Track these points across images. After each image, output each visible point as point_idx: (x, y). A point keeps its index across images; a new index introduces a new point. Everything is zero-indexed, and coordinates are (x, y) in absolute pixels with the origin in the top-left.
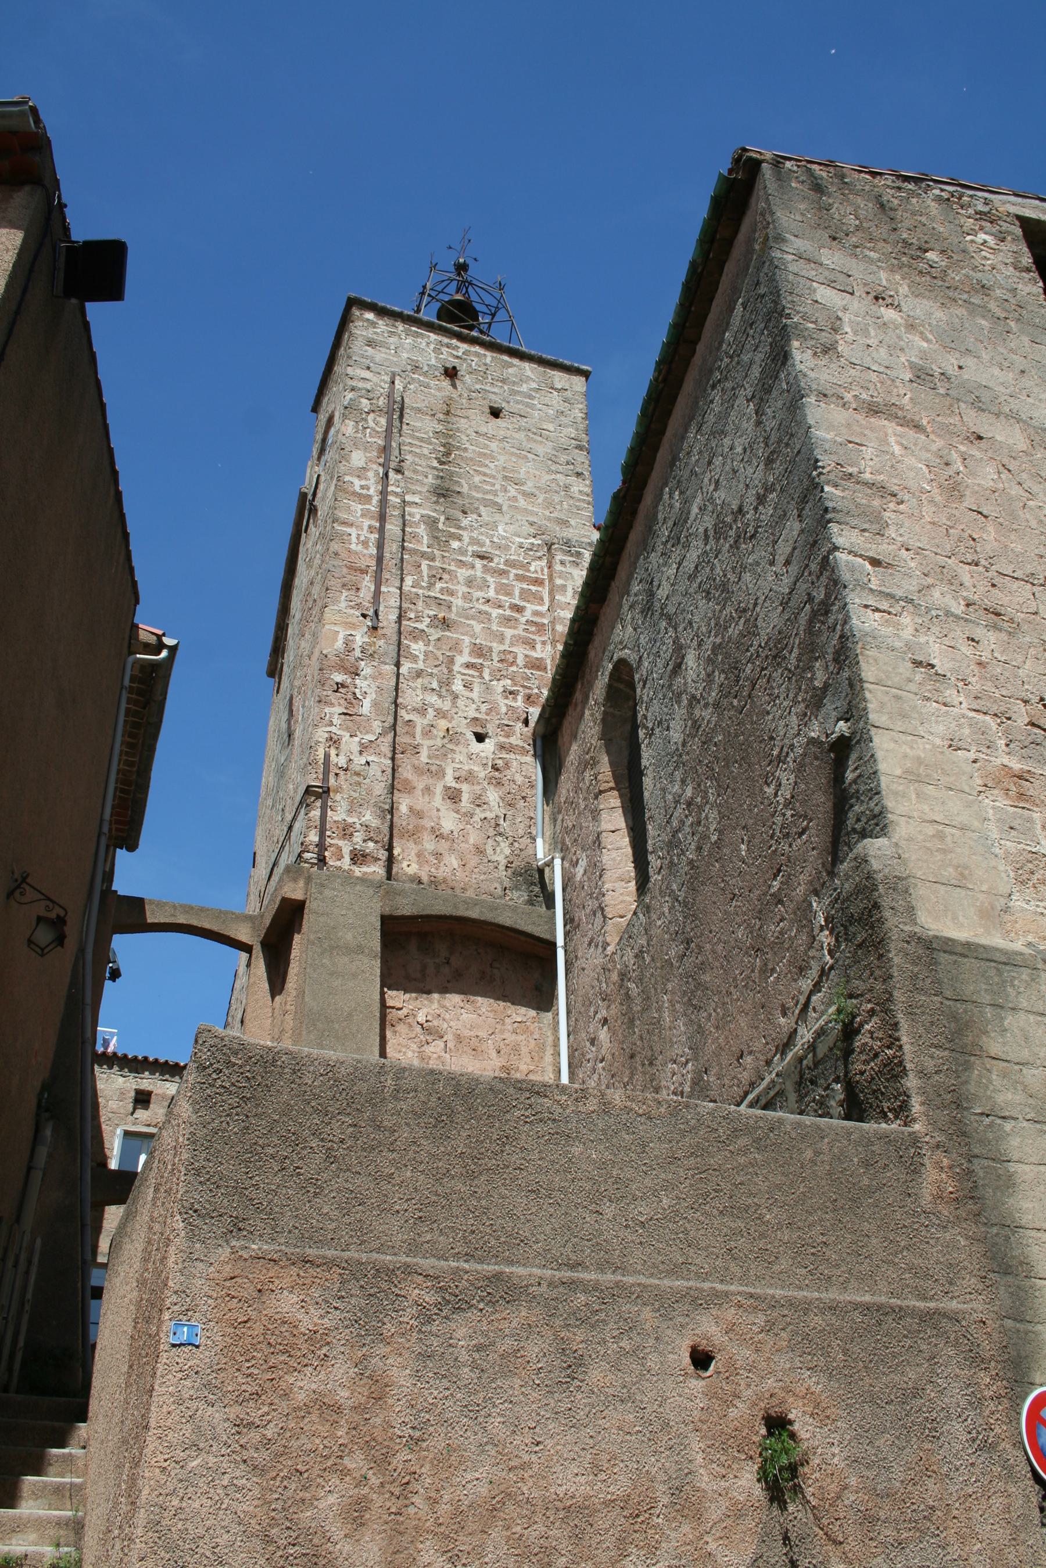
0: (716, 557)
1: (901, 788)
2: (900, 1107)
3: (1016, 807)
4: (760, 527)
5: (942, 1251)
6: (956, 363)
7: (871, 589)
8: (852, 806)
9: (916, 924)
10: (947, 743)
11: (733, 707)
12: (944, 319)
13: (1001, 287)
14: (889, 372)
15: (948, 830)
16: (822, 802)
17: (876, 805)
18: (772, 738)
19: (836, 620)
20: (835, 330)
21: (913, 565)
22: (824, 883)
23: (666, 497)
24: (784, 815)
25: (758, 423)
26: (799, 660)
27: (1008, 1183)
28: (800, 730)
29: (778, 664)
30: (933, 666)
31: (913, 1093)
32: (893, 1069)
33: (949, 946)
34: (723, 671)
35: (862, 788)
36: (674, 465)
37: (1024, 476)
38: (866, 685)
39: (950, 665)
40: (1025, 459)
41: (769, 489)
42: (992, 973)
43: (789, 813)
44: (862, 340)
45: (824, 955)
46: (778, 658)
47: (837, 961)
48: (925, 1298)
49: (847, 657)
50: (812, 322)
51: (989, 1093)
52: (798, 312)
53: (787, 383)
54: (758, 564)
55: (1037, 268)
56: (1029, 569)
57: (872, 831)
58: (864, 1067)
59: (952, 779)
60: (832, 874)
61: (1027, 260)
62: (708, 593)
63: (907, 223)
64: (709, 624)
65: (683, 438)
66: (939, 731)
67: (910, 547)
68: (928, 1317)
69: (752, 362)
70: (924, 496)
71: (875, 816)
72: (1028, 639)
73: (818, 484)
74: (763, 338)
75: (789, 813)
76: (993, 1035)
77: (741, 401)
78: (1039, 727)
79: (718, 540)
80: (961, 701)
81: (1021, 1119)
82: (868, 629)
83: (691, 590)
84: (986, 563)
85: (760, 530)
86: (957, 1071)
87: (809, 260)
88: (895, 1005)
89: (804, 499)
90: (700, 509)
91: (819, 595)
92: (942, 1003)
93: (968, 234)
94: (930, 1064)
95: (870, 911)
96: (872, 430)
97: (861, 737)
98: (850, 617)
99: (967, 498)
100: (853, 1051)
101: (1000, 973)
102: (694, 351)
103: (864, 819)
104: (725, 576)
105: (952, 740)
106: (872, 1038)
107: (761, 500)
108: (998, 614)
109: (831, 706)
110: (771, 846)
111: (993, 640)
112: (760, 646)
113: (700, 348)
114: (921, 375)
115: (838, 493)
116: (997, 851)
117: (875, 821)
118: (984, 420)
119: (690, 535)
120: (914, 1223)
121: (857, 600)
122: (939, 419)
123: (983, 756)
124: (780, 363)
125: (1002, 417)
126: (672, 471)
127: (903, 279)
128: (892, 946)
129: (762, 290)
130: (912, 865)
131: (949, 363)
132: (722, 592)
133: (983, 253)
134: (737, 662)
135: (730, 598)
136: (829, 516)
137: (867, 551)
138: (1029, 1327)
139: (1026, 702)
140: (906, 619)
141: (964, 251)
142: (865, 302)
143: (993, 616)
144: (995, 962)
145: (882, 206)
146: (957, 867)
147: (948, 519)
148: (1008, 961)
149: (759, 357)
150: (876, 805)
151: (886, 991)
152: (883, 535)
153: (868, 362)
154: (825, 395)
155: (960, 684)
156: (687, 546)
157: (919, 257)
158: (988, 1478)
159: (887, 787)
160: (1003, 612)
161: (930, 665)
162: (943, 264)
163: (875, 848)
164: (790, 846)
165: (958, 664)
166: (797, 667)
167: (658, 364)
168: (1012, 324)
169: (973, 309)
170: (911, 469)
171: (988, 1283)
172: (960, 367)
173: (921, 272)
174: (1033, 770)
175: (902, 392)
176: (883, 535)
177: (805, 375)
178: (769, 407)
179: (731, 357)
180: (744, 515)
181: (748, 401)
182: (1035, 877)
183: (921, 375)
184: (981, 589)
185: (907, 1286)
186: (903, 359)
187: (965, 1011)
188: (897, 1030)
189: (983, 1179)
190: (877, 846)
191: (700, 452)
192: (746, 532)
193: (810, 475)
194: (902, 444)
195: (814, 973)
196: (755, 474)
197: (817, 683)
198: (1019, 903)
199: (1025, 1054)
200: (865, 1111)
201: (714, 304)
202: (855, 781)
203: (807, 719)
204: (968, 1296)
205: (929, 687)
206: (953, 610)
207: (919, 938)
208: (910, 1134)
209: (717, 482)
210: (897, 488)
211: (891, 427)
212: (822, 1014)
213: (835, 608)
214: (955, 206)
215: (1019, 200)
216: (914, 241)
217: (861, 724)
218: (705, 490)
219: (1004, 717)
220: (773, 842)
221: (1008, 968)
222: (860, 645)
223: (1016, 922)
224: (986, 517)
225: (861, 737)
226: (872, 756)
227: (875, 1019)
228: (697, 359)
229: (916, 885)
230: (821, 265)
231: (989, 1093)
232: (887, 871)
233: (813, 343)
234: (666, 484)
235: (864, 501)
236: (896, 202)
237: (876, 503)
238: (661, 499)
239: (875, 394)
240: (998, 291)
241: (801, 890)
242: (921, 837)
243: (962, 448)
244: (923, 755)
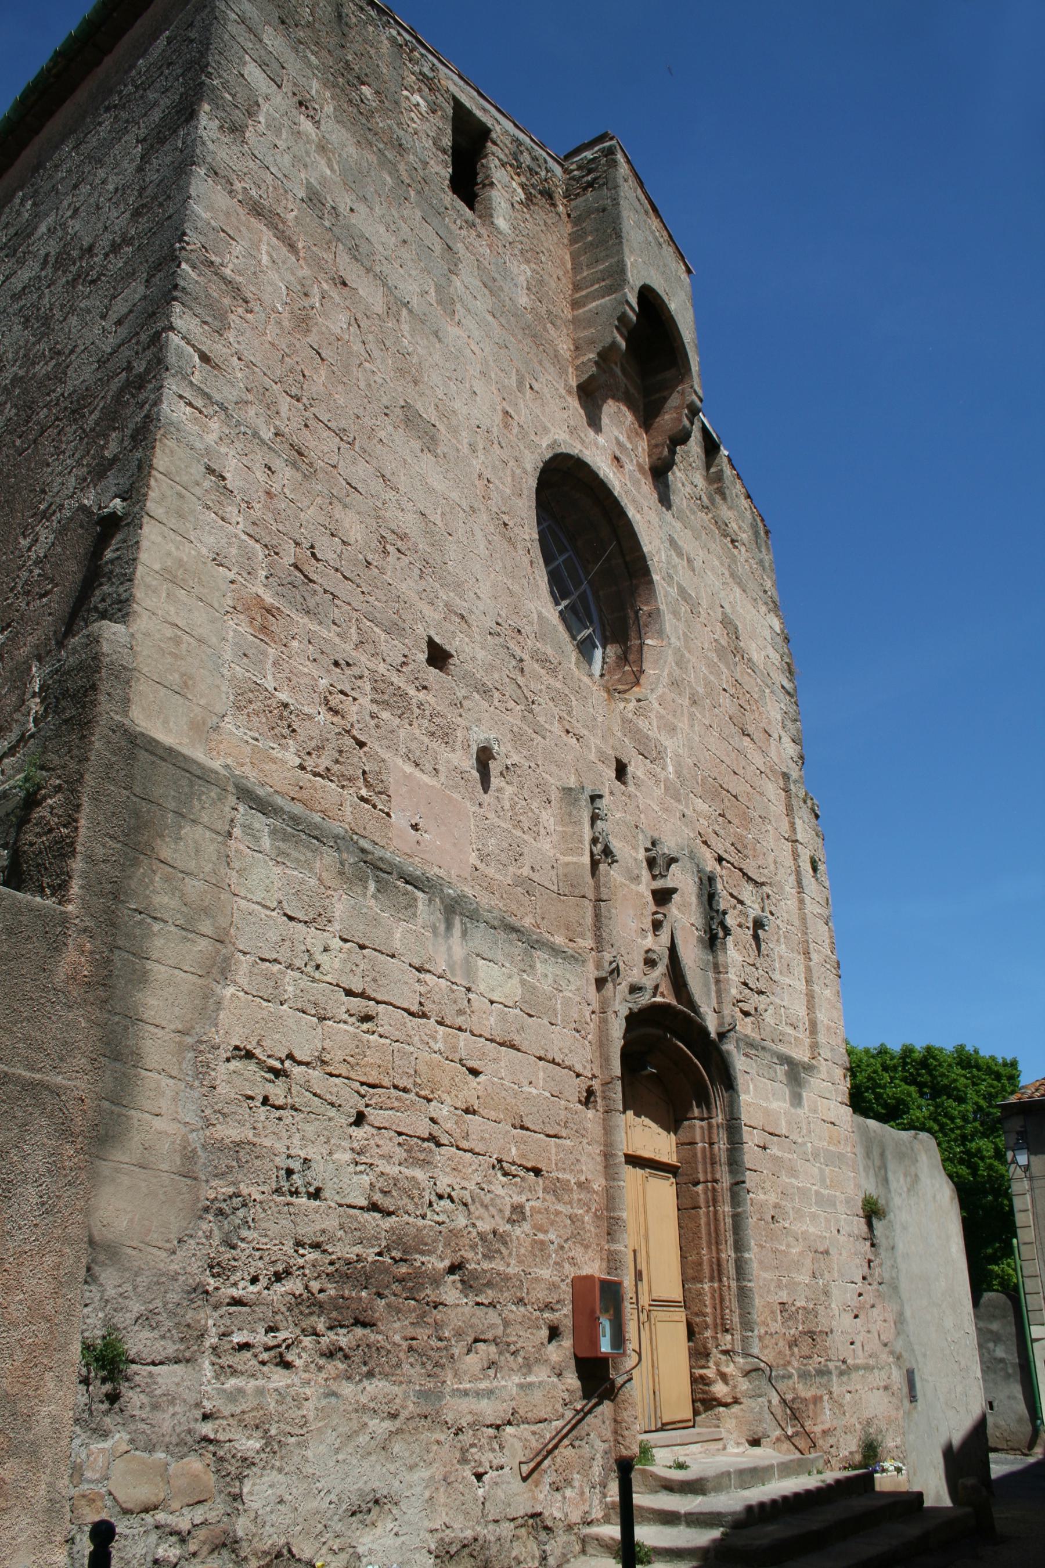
0: (49, 287)
1: (154, 583)
2: (60, 885)
3: (256, 637)
4: (104, 275)
5: (61, 1028)
6: (349, 203)
7: (191, 382)
8: (101, 584)
9: (127, 716)
10: (212, 556)
11: (15, 446)
12: (355, 157)
13: (415, 154)
14: (285, 181)
15: (186, 637)
16: (73, 570)
17: (125, 591)
18: (43, 491)
19: (147, 398)
20: (250, 114)
21: (239, 375)
22: (51, 651)
23: (17, 201)
24: (31, 571)
25: (140, 169)
26: (97, 424)
27: (142, 978)
28: (75, 493)
29: (75, 420)
30: (224, 479)
31: (76, 875)
32: (62, 848)
33: (152, 746)
34: (16, 406)
35: (117, 570)
36: (37, 171)
37: (370, 337)
38: (154, 472)
39: (241, 484)
40: (377, 322)
41: (127, 241)
42: (185, 782)
43: (37, 571)
44: (271, 137)
45: (28, 721)
46: (76, 413)
47: (40, 730)
48: (32, 1069)
49: (145, 438)
50: (230, 94)
51: (148, 892)
52: (220, 77)
53: (183, 143)
54: (89, 311)
55: (453, 154)
56: (343, 424)
57: (113, 614)
58: (35, 840)
59: (206, 591)
60: (60, 644)
61: (447, 142)
62: (27, 320)
63: (356, 47)
64: (17, 353)
65: (57, 147)
66: (208, 541)
67: (243, 358)
68: (30, 1087)
69: (156, 104)
70: (273, 315)
71: (120, 602)
72: (319, 487)
73: (177, 257)
74: (176, 84)
75: (37, 571)
76: (167, 840)
77: (130, 138)
78: (301, 571)
79: (56, 270)
80: (239, 523)
81: (170, 923)
82: (175, 420)
83: (10, 310)
84: (307, 403)
85: (103, 278)
86: (124, 864)
87: (250, 29)
88: (83, 787)
89: (158, 267)
90: (49, 230)
91: (140, 367)
92: (128, 798)
93: (406, 89)
94: (100, 852)
95: (86, 691)
96: (248, 228)
97: (133, 520)
98: (161, 401)
99: (313, 335)
100: (29, 821)
101: (191, 785)
102: (99, 63)
103: (109, 601)
104: (51, 310)
105: (218, 554)
106: (51, 813)
107: (115, 248)
108: (301, 454)
109: (112, 480)
110: (8, 599)
111: (288, 475)
112: (63, 395)
113: (108, 61)
114: (313, 199)
115: (193, 275)
116: (225, 672)
117: (119, 606)
118: (355, 269)
119: (29, 252)
120: (41, 997)
121: (174, 387)
122: (314, 249)
123: (242, 580)
124: (183, 118)
125: (371, 274)
126: (32, 176)
127: (332, 98)
128: (97, 730)
129: (193, 35)
130: (141, 659)
131: (345, 201)
132: (43, 325)
133: (412, 114)
134: (33, 402)
135: (48, 334)
136: (176, 294)
137: (202, 343)
138: (124, 1111)
139: (297, 544)
140: (215, 425)
141: (396, 103)
142: (288, 102)
143: (295, 454)
144: (190, 773)
145: (340, 16)
146: (183, 675)
147: (288, 347)
148: (202, 776)
149: (165, 102)
150: (125, 591)
151: (78, 772)
152: (221, 335)
153: (269, 161)
154: (216, 173)
155: (244, 505)
156: (21, 262)
157: (354, 85)
158: (46, 1238)
159: (142, 577)
160: (306, 454)
161: (222, 476)
162: (374, 104)
163: (111, 632)
164: (28, 604)
165: (248, 486)
166: (93, 430)
167: (58, 54)
168: (412, 193)
169: (384, 162)
170: (272, 284)
171: (97, 1065)
172: (352, 210)
173: (350, 101)
174: (282, 608)
175: (290, 206)
176: (221, 335)
177: (204, 143)
178: (157, 158)
179: (137, 87)
180: (92, 256)
181: (138, 141)
182: (252, 707)
183: (313, 199)
184: (294, 425)
185: (19, 1055)
186: (303, 176)
187: (148, 811)
188: (78, 812)
189: (119, 970)
190: (113, 630)
191: (70, 171)
192: (88, 275)
193: (172, 245)
194: (271, 256)
195: (13, 736)
196: (118, 219)
197: (106, 453)
198: (229, 726)
199: (192, 865)
200: (24, 881)
201: (139, 22)
202: (112, 561)
203: (85, 484)
204: (74, 1074)
205: (213, 497)
206: (261, 433)
207: (125, 730)
208: (62, 913)
209: (76, 211)
210: (251, 295)
211: (267, 235)
212: (10, 778)
213: (150, 386)
214: (404, 56)
215: (462, 83)
216: (356, 68)
217: (136, 509)
218: (60, 213)
219: (272, 550)
220: (12, 595)
221: (200, 782)
222: (162, 431)
223: (221, 742)
224: (322, 359)
225: (133, 520)
226: (137, 542)
227: (59, 796)
228: (100, 72)
229: (139, 680)
230: (261, 41)
231: (148, 892)
232: (115, 657)
233: (224, 115)
234: (21, 188)
235: (215, 294)
236: (354, 20)
237: (227, 301)
238: (10, 201)
239: (265, 196)
240: (411, 157)
241: (24, 651)
242: (158, 636)
243: (325, 286)
244: (185, 559)
